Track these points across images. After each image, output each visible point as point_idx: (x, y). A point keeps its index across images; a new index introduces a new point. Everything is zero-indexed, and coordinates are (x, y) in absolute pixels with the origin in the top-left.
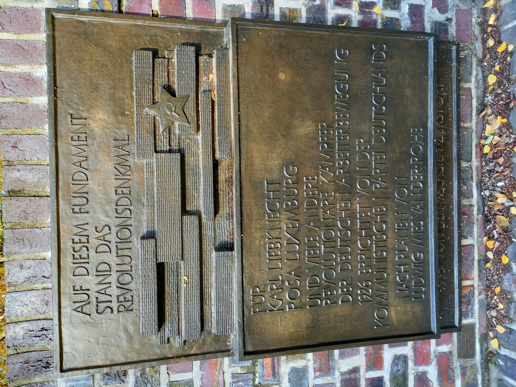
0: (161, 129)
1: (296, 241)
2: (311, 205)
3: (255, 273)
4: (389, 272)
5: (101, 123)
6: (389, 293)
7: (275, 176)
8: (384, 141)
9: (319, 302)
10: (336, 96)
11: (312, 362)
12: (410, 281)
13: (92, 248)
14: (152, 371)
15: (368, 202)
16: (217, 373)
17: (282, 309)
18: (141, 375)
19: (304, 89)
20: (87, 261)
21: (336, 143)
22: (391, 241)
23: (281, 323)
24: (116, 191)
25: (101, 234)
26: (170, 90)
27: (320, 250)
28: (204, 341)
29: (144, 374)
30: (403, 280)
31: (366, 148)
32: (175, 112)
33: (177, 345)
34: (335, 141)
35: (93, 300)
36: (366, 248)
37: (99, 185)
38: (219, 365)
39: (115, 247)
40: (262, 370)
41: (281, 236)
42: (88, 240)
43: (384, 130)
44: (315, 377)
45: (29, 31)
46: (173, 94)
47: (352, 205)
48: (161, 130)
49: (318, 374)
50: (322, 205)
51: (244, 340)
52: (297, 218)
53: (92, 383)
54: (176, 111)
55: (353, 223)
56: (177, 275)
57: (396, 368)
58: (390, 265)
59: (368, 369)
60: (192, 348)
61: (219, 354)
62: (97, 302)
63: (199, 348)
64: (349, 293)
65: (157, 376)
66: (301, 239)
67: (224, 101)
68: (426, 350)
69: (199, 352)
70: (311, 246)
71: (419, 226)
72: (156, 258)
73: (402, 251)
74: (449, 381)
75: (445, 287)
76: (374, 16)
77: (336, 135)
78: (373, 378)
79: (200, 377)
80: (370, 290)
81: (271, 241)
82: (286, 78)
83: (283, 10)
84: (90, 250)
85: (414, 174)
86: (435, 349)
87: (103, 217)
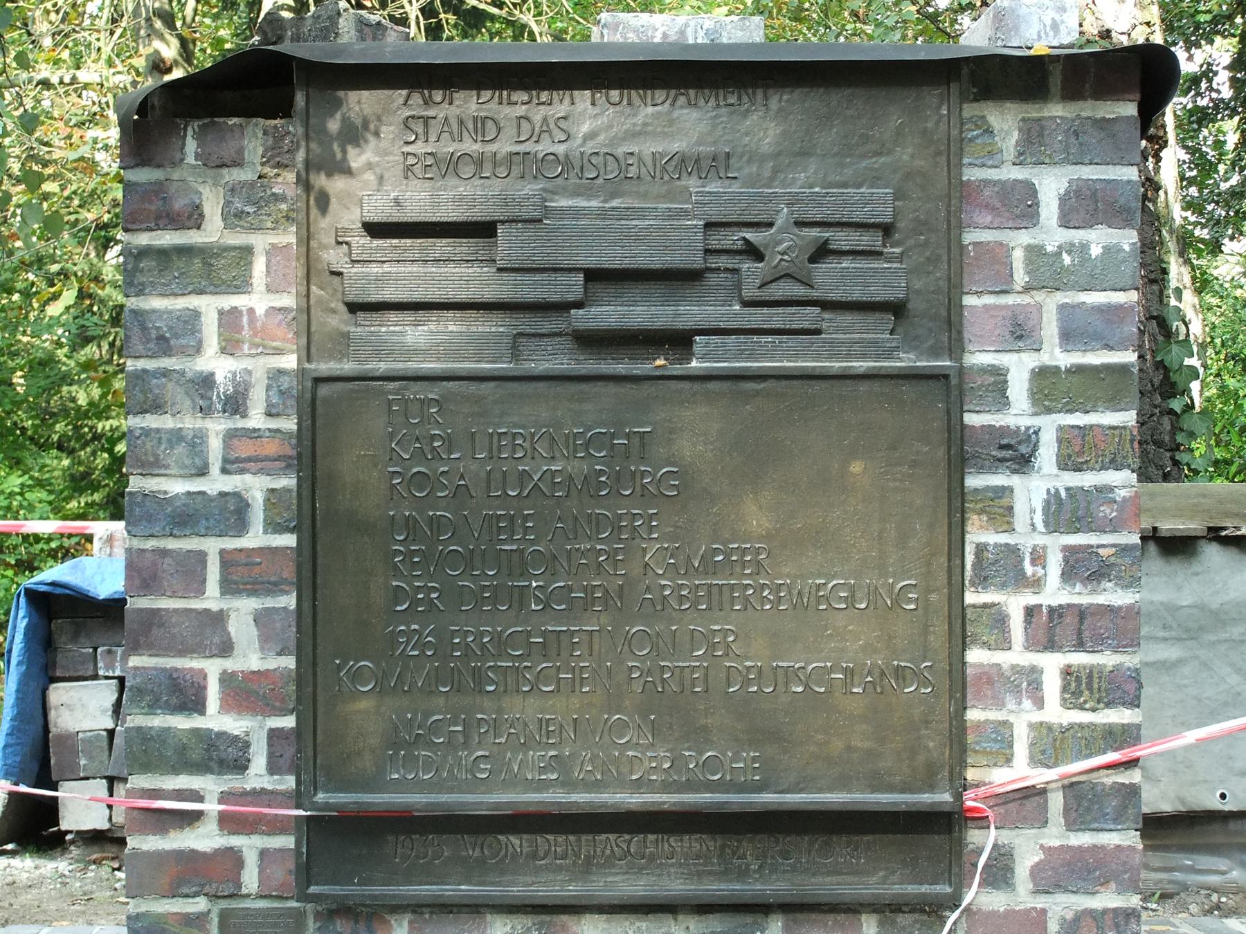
1: (527, 491)
8: (731, 690)
9: (401, 538)
13: (527, 110)
14: (280, 216)
18: (274, 194)
20: (505, 102)
21: (726, 579)
23: (365, 455)
24: (632, 154)
25: (552, 126)
26: (822, 252)
28: (334, 311)
29: (276, 200)
32: (782, 260)
35: (431, 113)
37: (645, 124)
39: (527, 150)
42: (543, 103)
43: (755, 689)
46: (813, 259)
48: (748, 236)
50: (598, 547)
52: (574, 493)
54: (783, 263)
56: (468, 261)
60: (322, 289)
61: (304, 341)
62: (428, 118)
63: (320, 301)
65: (269, 225)
69: (312, 301)
72: (507, 221)
76: (1011, 704)
77: (741, 580)
78: (205, 688)
80: (416, 653)
81: (528, 439)
83: (1007, 493)
84: (524, 107)
87: (585, 128)
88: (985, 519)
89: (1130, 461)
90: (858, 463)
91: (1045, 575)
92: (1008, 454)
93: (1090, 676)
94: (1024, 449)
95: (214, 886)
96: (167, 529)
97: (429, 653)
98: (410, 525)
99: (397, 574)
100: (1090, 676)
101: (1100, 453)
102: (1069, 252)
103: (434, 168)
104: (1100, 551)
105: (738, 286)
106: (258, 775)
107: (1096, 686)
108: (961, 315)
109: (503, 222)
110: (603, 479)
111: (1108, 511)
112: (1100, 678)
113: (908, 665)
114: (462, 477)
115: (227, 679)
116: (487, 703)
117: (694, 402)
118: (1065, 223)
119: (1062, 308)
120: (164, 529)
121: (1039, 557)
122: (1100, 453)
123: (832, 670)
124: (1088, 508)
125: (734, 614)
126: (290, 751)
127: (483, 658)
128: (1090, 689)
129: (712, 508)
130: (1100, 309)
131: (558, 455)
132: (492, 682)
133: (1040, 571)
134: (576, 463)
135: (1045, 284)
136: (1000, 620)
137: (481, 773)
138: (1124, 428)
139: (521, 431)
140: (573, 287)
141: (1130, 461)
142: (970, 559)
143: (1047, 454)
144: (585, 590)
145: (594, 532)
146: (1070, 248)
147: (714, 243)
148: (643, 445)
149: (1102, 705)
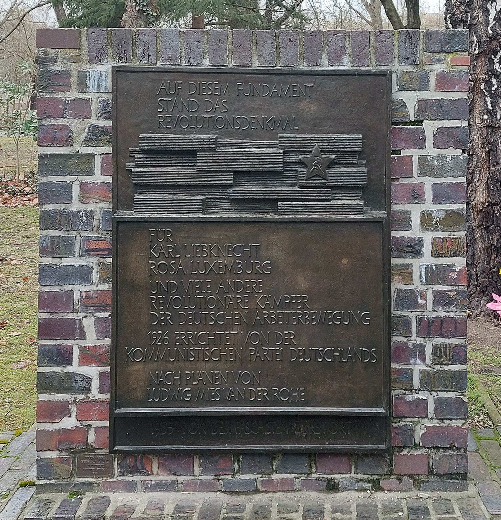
2: (237, 285)
3: (183, 233)
4: (175, 363)
5: (307, 108)
6: (156, 363)
7: (263, 253)
10: (331, 312)
11: (96, 289)
12: (166, 386)
14: (106, 141)
15: (239, 342)
16: (97, 197)
17: (151, 257)
19: (335, 281)
22: (203, 367)
26: (332, 164)
27: (198, 294)
30: (168, 377)
31: (286, 341)
32: (314, 168)
34: (292, 310)
36: (197, 339)
38: (104, 199)
40: (94, 239)
41: (213, 257)
43: (302, 360)
44: (81, 292)
45: (49, 374)
46: (329, 167)
47: (236, 326)
49: (84, 294)
52: (228, 273)
53: (102, 91)
55: (221, 327)
57: (79, 379)
58: (181, 364)
59: (81, 349)
64: (160, 321)
68: (92, 415)
70: (202, 287)
71: (215, 396)
73: (193, 377)
74: (57, 443)
75: (154, 435)
76: (412, 361)
79: (95, 182)
80: (160, 344)
82: (344, 265)
85: (262, 390)
86: (92, 426)
88: (401, 278)
89: (462, 253)
90: (345, 259)
91: (426, 303)
95: (75, 445)
96: (57, 282)
97: (166, 344)
99: (153, 309)
100: (445, 349)
101: (450, 249)
102: (437, 160)
103: (171, 123)
104: (449, 293)
106: (95, 393)
107: (448, 353)
109: (199, 150)
110: (239, 266)
111: (453, 276)
112: (450, 350)
113: (366, 349)
114: (180, 265)
115: (82, 349)
117: (278, 233)
118: (436, 146)
119: (434, 184)
120: (55, 282)
121: (423, 296)
122: (450, 249)
123: (334, 351)
124: (444, 274)
125: (293, 325)
126: (108, 382)
128: (446, 355)
129: (285, 279)
130: (451, 185)
131: (221, 255)
132: (192, 357)
133: (424, 302)
135: (427, 174)
136: (407, 323)
137: (187, 398)
138: (460, 238)
139: (205, 245)
140: (229, 179)
141: (462, 253)
143: (427, 249)
145: (261, 93)
146: (438, 157)
148: (257, 251)
149: (450, 362)
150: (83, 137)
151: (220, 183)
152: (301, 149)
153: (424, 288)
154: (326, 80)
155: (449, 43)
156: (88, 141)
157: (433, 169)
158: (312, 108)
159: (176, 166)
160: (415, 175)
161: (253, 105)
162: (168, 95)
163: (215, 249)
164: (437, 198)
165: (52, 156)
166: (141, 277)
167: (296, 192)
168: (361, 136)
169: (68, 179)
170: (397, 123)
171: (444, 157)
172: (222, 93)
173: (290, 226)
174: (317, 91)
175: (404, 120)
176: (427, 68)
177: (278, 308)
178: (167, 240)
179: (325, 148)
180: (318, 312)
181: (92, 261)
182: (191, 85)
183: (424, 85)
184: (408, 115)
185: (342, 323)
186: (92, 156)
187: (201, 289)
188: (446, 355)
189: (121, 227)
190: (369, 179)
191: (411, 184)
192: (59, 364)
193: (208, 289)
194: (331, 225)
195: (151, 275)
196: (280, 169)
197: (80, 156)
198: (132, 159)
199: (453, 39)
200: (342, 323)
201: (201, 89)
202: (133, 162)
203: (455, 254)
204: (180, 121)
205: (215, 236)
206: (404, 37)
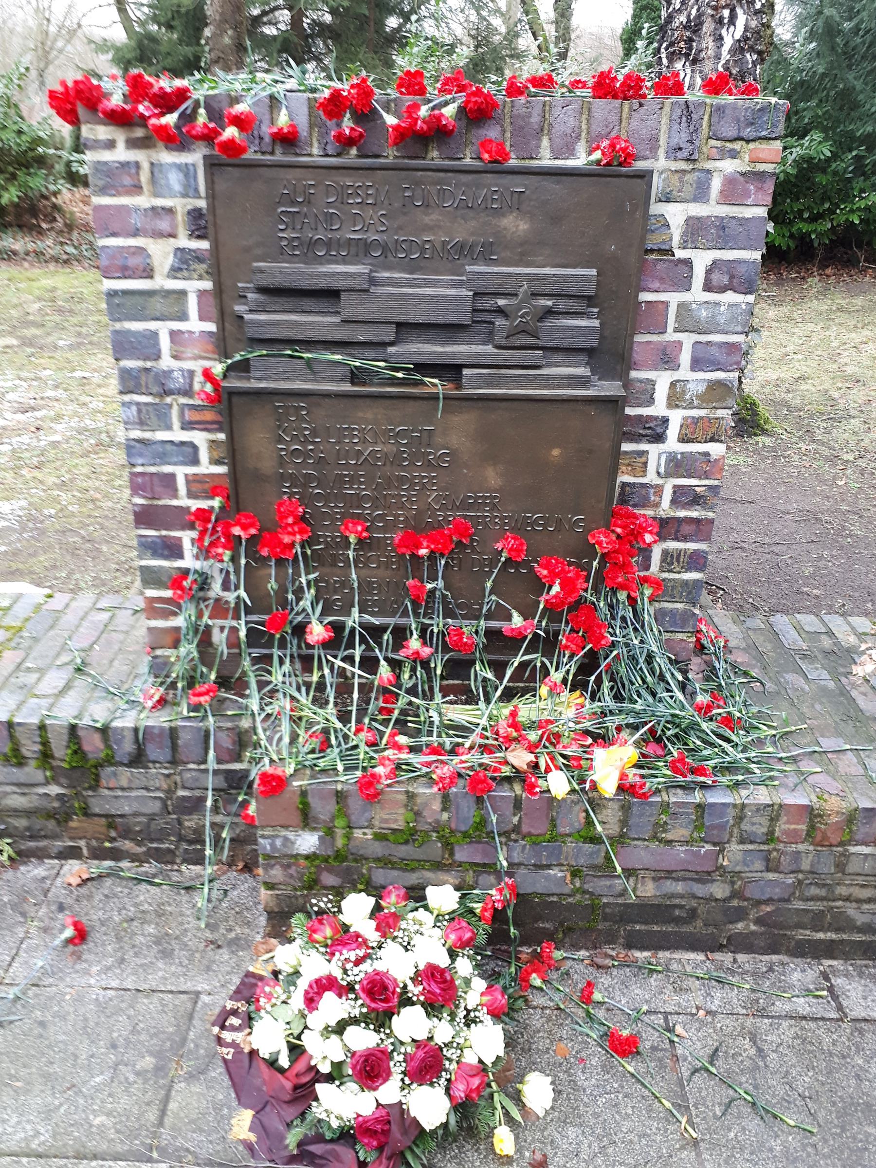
0: (501, 302)
2: (402, 480)
7: (438, 440)
17: (280, 440)
26: (549, 312)
33: (237, 308)
46: (541, 319)
51: (283, 394)
52: (388, 464)
55: (379, 530)
58: (327, 570)
66: (362, 467)
67: (532, 381)
70: (354, 479)
92: (648, 432)
93: (679, 555)
94: (659, 430)
98: (293, 478)
100: (679, 555)
105: (491, 333)
108: (631, 348)
109: (344, 291)
116: (339, 571)
121: (659, 490)
127: (337, 549)
128: (678, 561)
133: (658, 499)
134: (389, 446)
140: (388, 333)
142: (617, 490)
143: (673, 432)
144: (394, 515)
147: (479, 306)
148: (430, 437)
150: (167, 268)
151: (375, 339)
152: (502, 290)
153: (660, 481)
154: (549, 184)
155: (752, 124)
156: (175, 272)
157: (698, 321)
158: (521, 227)
159: (310, 312)
160: (670, 329)
161: (427, 220)
162: (293, 203)
163: (370, 433)
164: (697, 364)
165: (126, 293)
166: (268, 465)
167: (491, 355)
168: (594, 272)
169: (152, 325)
170: (652, 251)
171: (718, 304)
172: (379, 202)
173: (480, 404)
174: (531, 200)
175: (663, 247)
176: (709, 165)
177: (458, 509)
178: (301, 419)
179: (540, 291)
180: (513, 515)
181: (200, 438)
182: (330, 188)
183: (700, 194)
184: (671, 240)
185: (545, 528)
186: (183, 293)
187: (351, 482)
188: (678, 561)
189: (235, 399)
190: (602, 337)
191: (660, 343)
192: (166, 558)
193: (361, 483)
194: (540, 404)
195: (281, 462)
196: (466, 320)
197: (168, 293)
198: (243, 300)
199: (759, 118)
200: (545, 528)
201: (345, 196)
202: (245, 304)
203: (712, 440)
204: (313, 244)
205: (369, 415)
206: (679, 112)
